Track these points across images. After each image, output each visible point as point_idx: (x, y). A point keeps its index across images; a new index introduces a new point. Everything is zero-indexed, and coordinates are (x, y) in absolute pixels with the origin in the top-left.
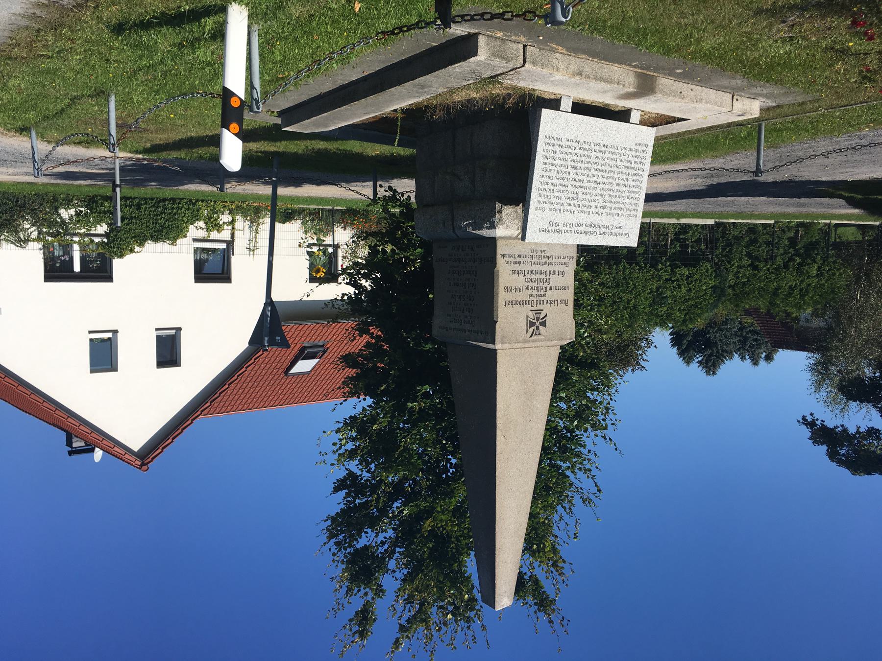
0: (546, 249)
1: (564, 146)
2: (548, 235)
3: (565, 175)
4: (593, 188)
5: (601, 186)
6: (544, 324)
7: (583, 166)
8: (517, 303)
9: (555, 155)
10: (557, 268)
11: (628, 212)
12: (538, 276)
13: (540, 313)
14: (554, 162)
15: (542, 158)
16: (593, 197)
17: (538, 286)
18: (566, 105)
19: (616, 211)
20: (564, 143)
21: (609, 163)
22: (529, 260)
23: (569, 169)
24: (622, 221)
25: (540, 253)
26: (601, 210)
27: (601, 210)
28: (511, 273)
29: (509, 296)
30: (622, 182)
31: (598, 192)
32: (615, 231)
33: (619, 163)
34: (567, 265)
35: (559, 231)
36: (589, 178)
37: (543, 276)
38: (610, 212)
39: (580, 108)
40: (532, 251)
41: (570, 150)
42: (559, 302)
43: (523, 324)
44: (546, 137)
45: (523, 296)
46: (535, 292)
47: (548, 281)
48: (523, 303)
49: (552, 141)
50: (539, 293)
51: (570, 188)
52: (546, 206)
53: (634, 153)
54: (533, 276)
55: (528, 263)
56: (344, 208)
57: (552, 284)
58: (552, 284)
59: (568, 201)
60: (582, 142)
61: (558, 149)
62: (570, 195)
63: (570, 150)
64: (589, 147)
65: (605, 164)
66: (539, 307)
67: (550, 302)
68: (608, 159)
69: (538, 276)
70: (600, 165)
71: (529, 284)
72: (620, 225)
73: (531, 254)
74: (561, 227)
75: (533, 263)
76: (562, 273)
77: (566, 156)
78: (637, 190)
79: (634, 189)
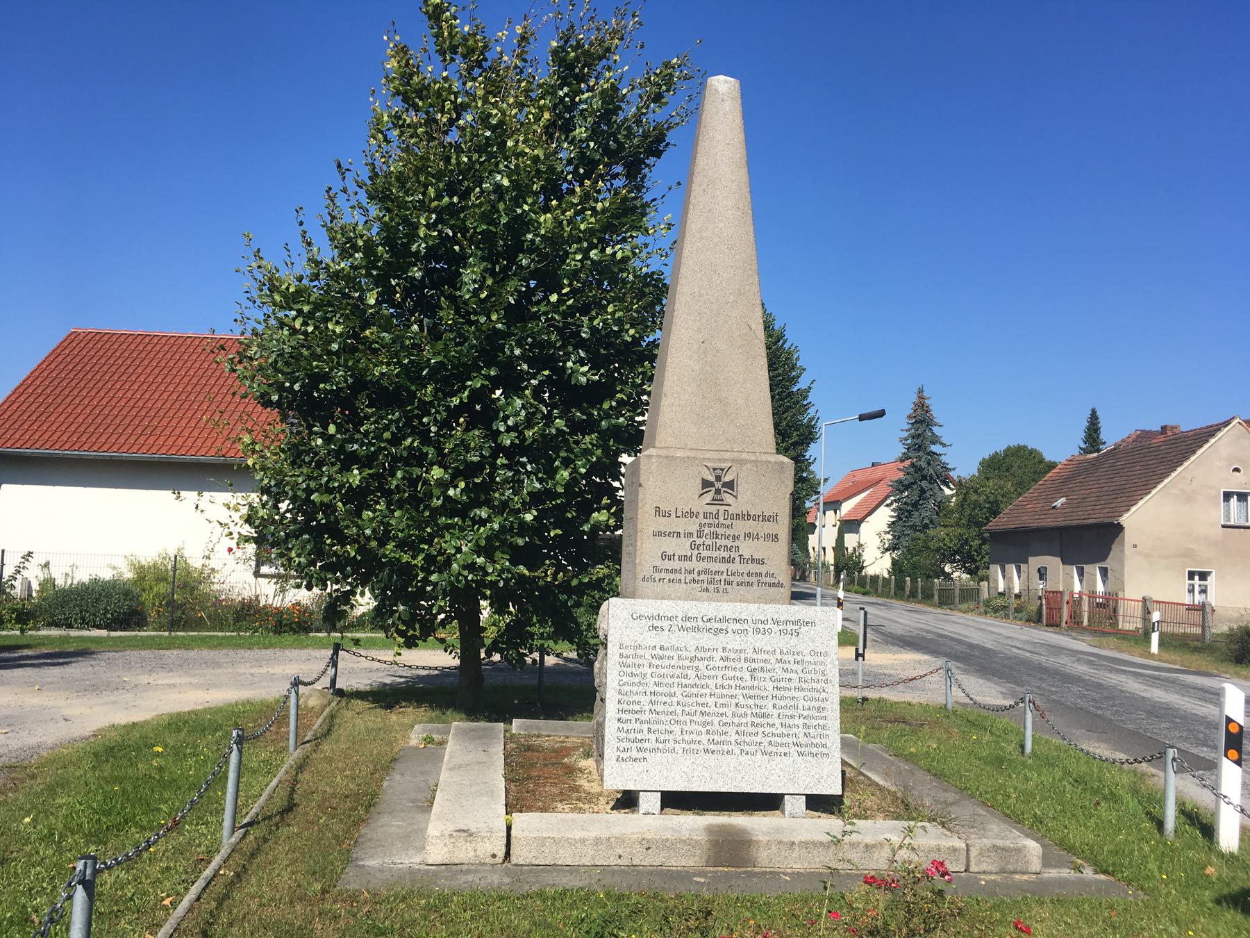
0: (699, 594)
1: (791, 745)
2: (797, 617)
3: (782, 703)
4: (723, 687)
5: (707, 691)
6: (706, 484)
7: (749, 719)
8: (755, 518)
9: (807, 731)
10: (676, 564)
11: (640, 652)
12: (715, 554)
13: (713, 500)
14: (805, 721)
15: (830, 724)
16: (720, 674)
17: (714, 540)
18: (795, 805)
19: (667, 653)
20: (793, 750)
21: (697, 727)
22: (732, 578)
23: (776, 712)
24: (650, 639)
25: (711, 587)
26: (699, 655)
27: (699, 655)
28: (765, 561)
29: (769, 528)
30: (664, 699)
31: (711, 683)
32: (666, 624)
33: (677, 728)
34: (656, 569)
35: (777, 622)
36: (734, 701)
37: (705, 553)
38: (680, 652)
39: (771, 802)
40: (726, 591)
41: (779, 740)
42: (673, 514)
43: (742, 488)
44: (827, 755)
45: (741, 527)
46: (721, 531)
47: (694, 546)
48: (743, 517)
49: (815, 750)
50: (712, 529)
51: (770, 685)
52: (808, 658)
53: (646, 745)
54: (726, 554)
55: (733, 574)
56: (311, 634)
57: (688, 542)
58: (688, 542)
59: (769, 667)
60: (759, 753)
61: (803, 740)
62: (767, 675)
63: (779, 740)
64: (742, 747)
65: (704, 724)
66: (714, 509)
67: (692, 514)
68: (700, 733)
69: (715, 554)
70: (716, 723)
71: (733, 544)
72: (655, 632)
73: (727, 586)
74: (776, 628)
75: (725, 574)
76: (664, 556)
77: (785, 731)
78: (627, 688)
79: (635, 689)
